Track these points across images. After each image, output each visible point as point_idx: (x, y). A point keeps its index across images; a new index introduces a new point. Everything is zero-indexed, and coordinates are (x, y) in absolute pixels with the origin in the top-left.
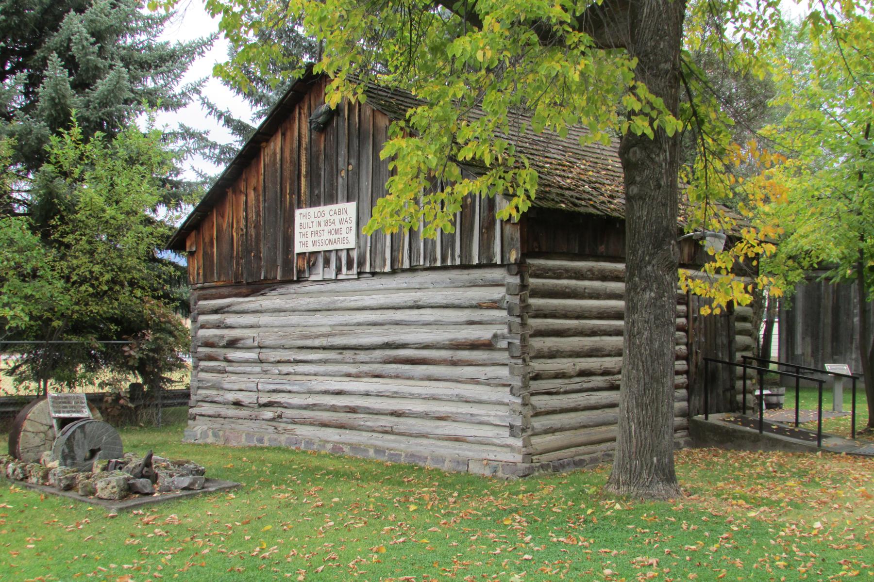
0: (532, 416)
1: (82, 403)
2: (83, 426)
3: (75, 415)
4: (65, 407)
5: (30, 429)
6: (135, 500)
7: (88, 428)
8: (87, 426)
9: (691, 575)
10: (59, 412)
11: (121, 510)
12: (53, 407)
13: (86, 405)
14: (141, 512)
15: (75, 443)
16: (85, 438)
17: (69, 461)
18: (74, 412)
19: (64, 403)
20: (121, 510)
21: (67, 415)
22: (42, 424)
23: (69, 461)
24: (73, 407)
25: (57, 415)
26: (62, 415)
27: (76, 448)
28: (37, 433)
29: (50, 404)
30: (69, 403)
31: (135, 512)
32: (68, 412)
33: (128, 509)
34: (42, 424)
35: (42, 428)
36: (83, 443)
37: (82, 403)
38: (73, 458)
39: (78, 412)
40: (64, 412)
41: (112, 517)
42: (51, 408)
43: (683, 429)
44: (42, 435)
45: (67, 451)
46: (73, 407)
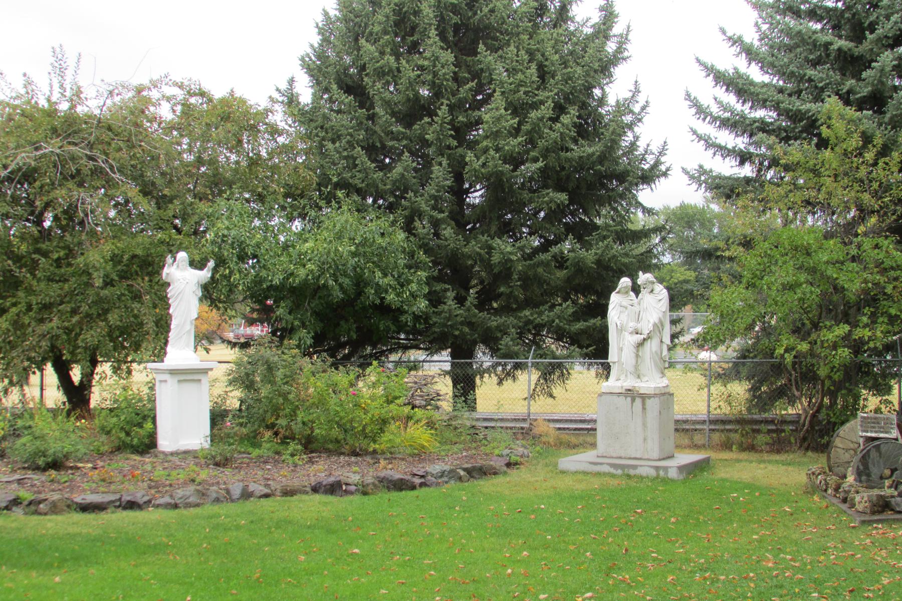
0: (473, 409)
1: (892, 424)
2: (879, 446)
3: (882, 435)
4: (874, 427)
5: (840, 445)
6: (888, 515)
7: (883, 448)
8: (882, 446)
9: (542, 596)
10: (867, 432)
11: (863, 522)
12: (861, 426)
13: (895, 426)
14: (880, 526)
15: (870, 461)
16: (880, 457)
17: (864, 478)
18: (882, 432)
19: (874, 423)
20: (863, 522)
21: (874, 435)
22: (852, 442)
23: (864, 478)
24: (881, 428)
25: (864, 434)
26: (869, 434)
27: (870, 466)
28: (847, 450)
29: (859, 423)
30: (878, 423)
31: (875, 525)
32: (876, 432)
33: (870, 522)
34: (852, 442)
35: (852, 446)
36: (878, 462)
37: (892, 424)
38: (868, 475)
39: (886, 432)
40: (871, 432)
41: (854, 527)
42: (859, 427)
43: (23, 390)
44: (852, 452)
45: (861, 467)
46: (881, 428)
